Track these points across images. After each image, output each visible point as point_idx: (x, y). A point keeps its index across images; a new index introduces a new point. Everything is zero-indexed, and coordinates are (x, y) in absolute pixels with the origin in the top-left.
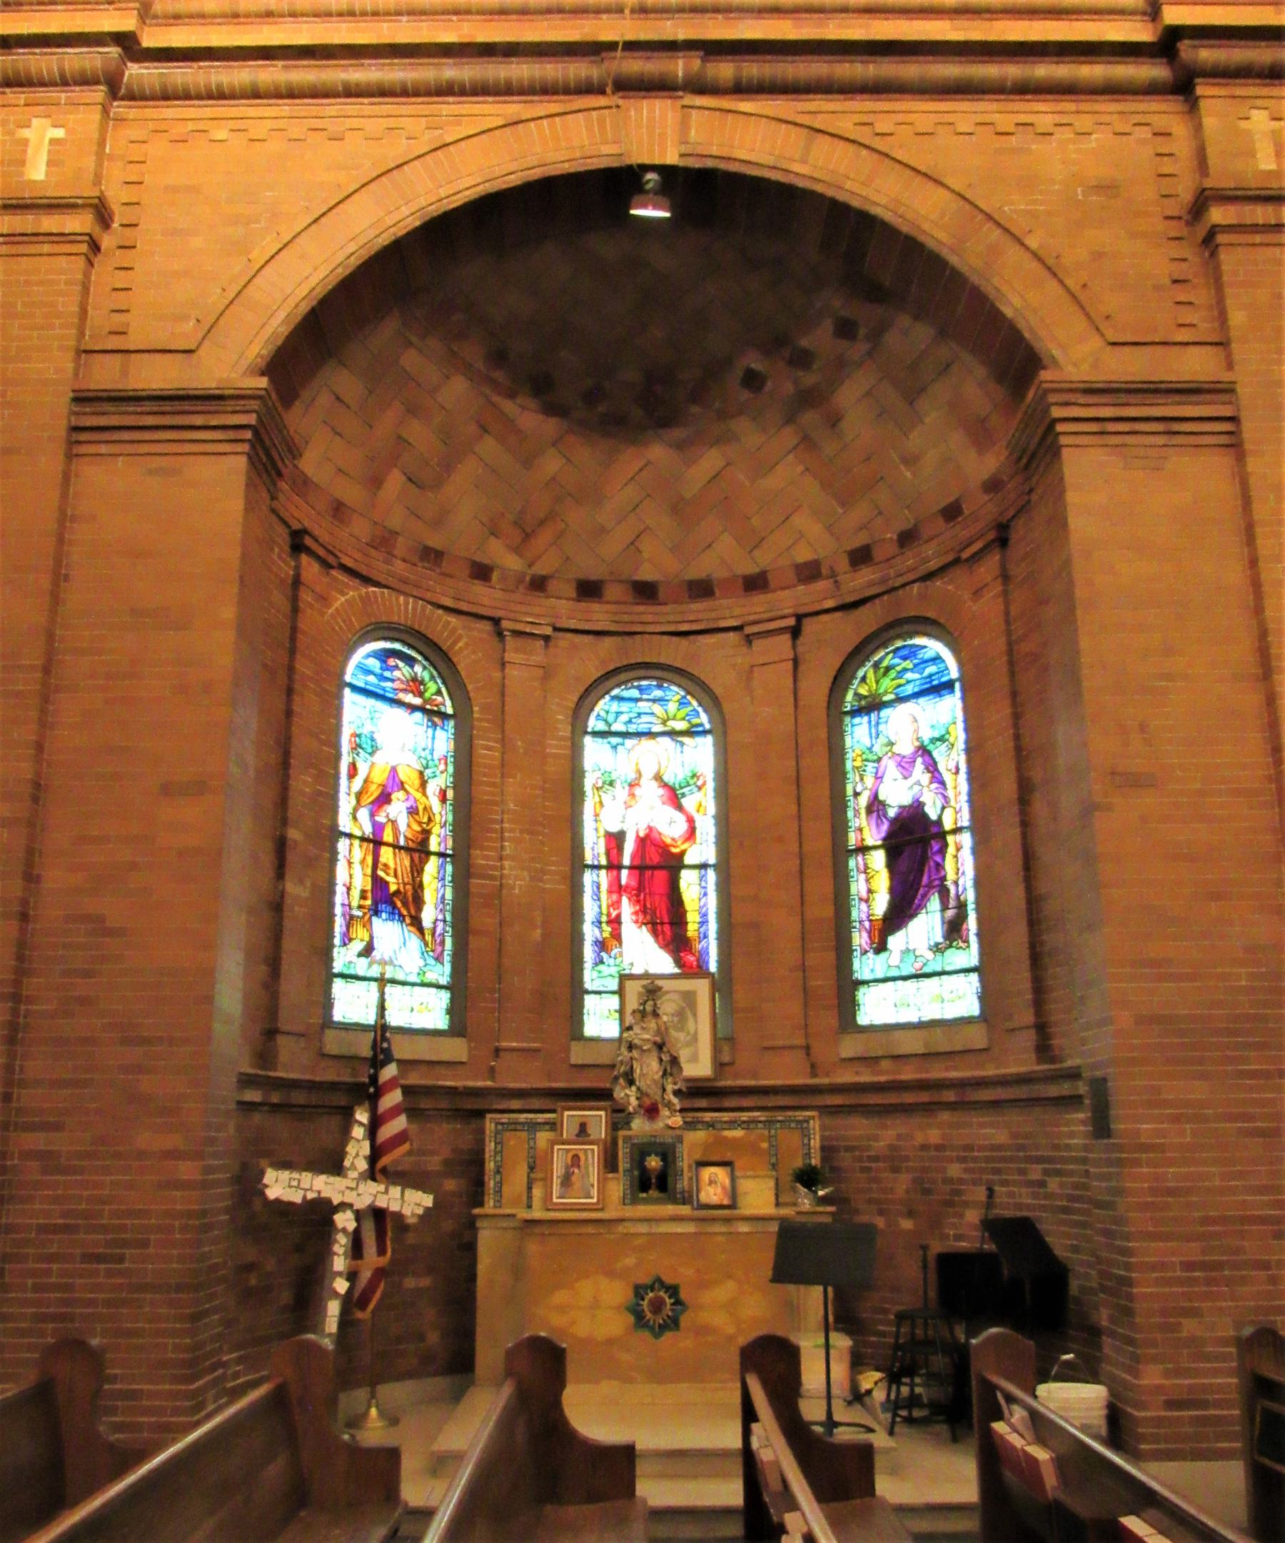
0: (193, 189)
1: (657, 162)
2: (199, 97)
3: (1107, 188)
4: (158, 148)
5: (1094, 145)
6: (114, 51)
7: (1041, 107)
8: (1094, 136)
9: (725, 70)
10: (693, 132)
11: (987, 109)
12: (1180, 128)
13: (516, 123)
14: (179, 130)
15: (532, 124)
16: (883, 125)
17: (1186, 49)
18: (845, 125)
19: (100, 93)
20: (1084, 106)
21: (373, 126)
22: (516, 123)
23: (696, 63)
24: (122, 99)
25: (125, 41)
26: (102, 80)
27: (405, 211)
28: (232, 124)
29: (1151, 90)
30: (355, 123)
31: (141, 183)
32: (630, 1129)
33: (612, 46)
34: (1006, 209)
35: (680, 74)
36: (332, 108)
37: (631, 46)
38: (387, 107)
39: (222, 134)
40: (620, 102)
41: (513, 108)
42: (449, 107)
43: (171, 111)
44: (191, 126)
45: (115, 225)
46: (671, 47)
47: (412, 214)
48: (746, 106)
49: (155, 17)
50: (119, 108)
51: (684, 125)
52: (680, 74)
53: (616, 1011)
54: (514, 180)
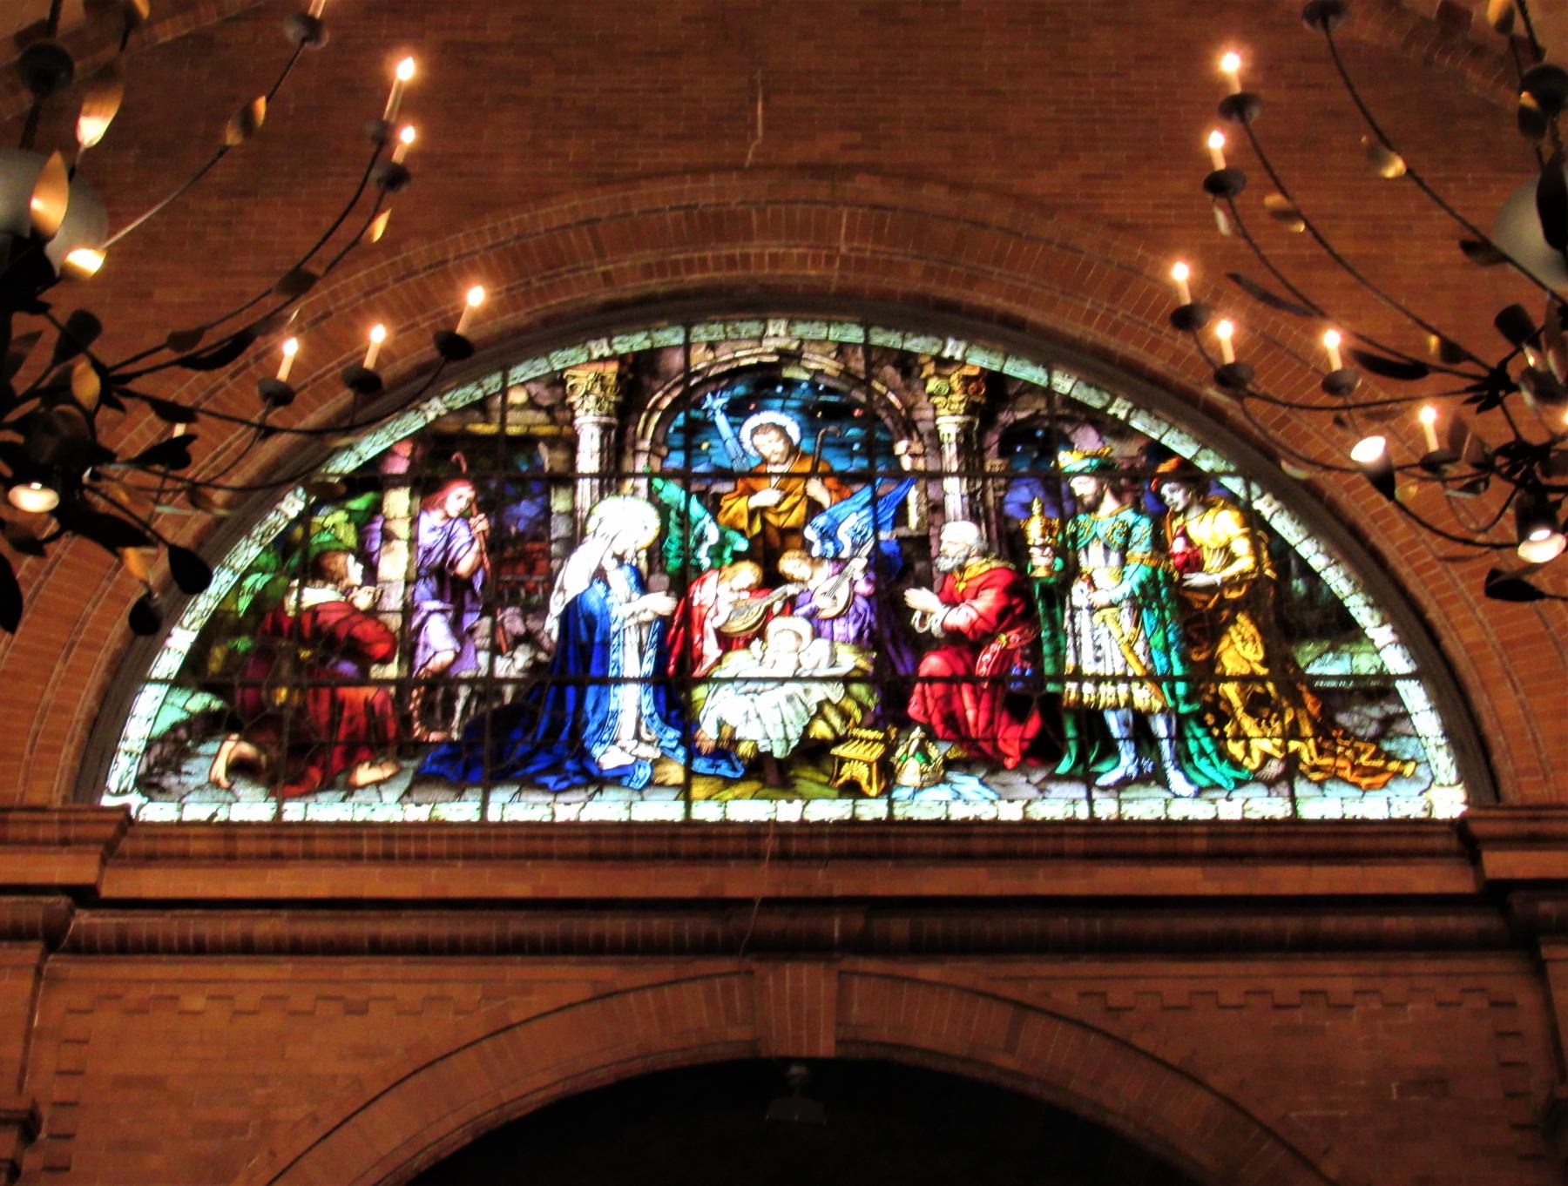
0: (154, 1082)
1: (805, 1053)
2: (169, 951)
3: (1433, 1083)
4: (105, 1021)
5: (1410, 1020)
6: (63, 901)
7: (1336, 967)
8: (1410, 1007)
9: (899, 927)
10: (855, 1009)
11: (1262, 970)
12: (1526, 997)
13: (609, 995)
14: (135, 995)
15: (631, 997)
16: (1117, 997)
17: (1516, 900)
18: (1067, 998)
19: (33, 951)
20: (1397, 966)
21: (411, 995)
22: (609, 995)
23: (858, 922)
24: (64, 951)
25: (84, 896)
26: (41, 935)
27: (452, 1122)
28: (212, 989)
29: (1481, 944)
30: (388, 989)
31: (81, 1073)
32: (1199, 759)
33: (746, 903)
34: (1293, 1115)
35: (836, 934)
36: (353, 969)
37: (770, 903)
38: (425, 969)
39: (197, 1002)
40: (755, 966)
41: (606, 972)
42: (516, 970)
43: (125, 969)
44: (153, 990)
45: (43, 1135)
46: (826, 903)
47: (462, 1126)
48: (929, 971)
49: (122, 856)
50: (55, 963)
51: (842, 1002)
52: (836, 934)
53: (1429, 808)
54: (605, 1076)
